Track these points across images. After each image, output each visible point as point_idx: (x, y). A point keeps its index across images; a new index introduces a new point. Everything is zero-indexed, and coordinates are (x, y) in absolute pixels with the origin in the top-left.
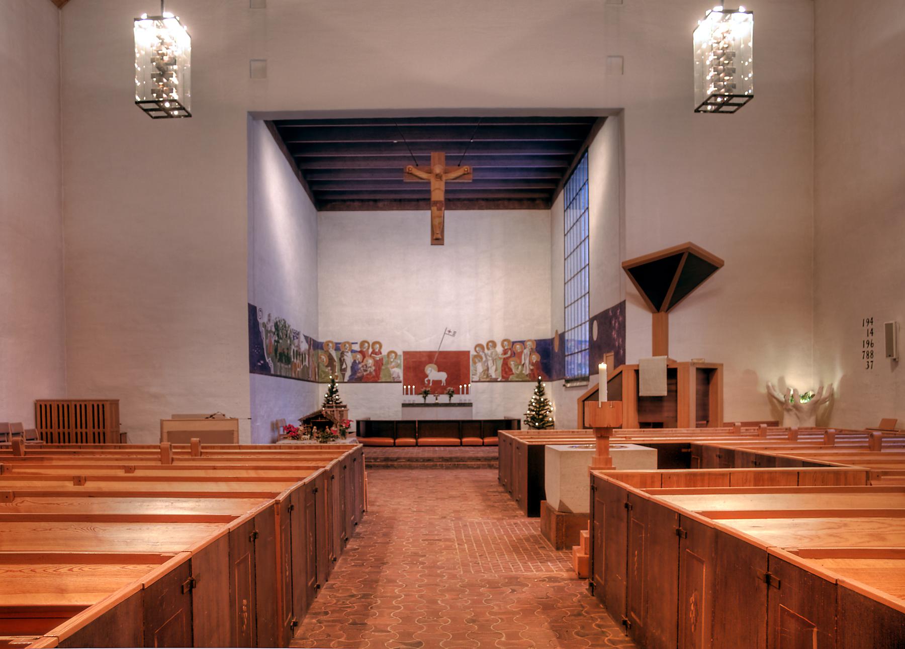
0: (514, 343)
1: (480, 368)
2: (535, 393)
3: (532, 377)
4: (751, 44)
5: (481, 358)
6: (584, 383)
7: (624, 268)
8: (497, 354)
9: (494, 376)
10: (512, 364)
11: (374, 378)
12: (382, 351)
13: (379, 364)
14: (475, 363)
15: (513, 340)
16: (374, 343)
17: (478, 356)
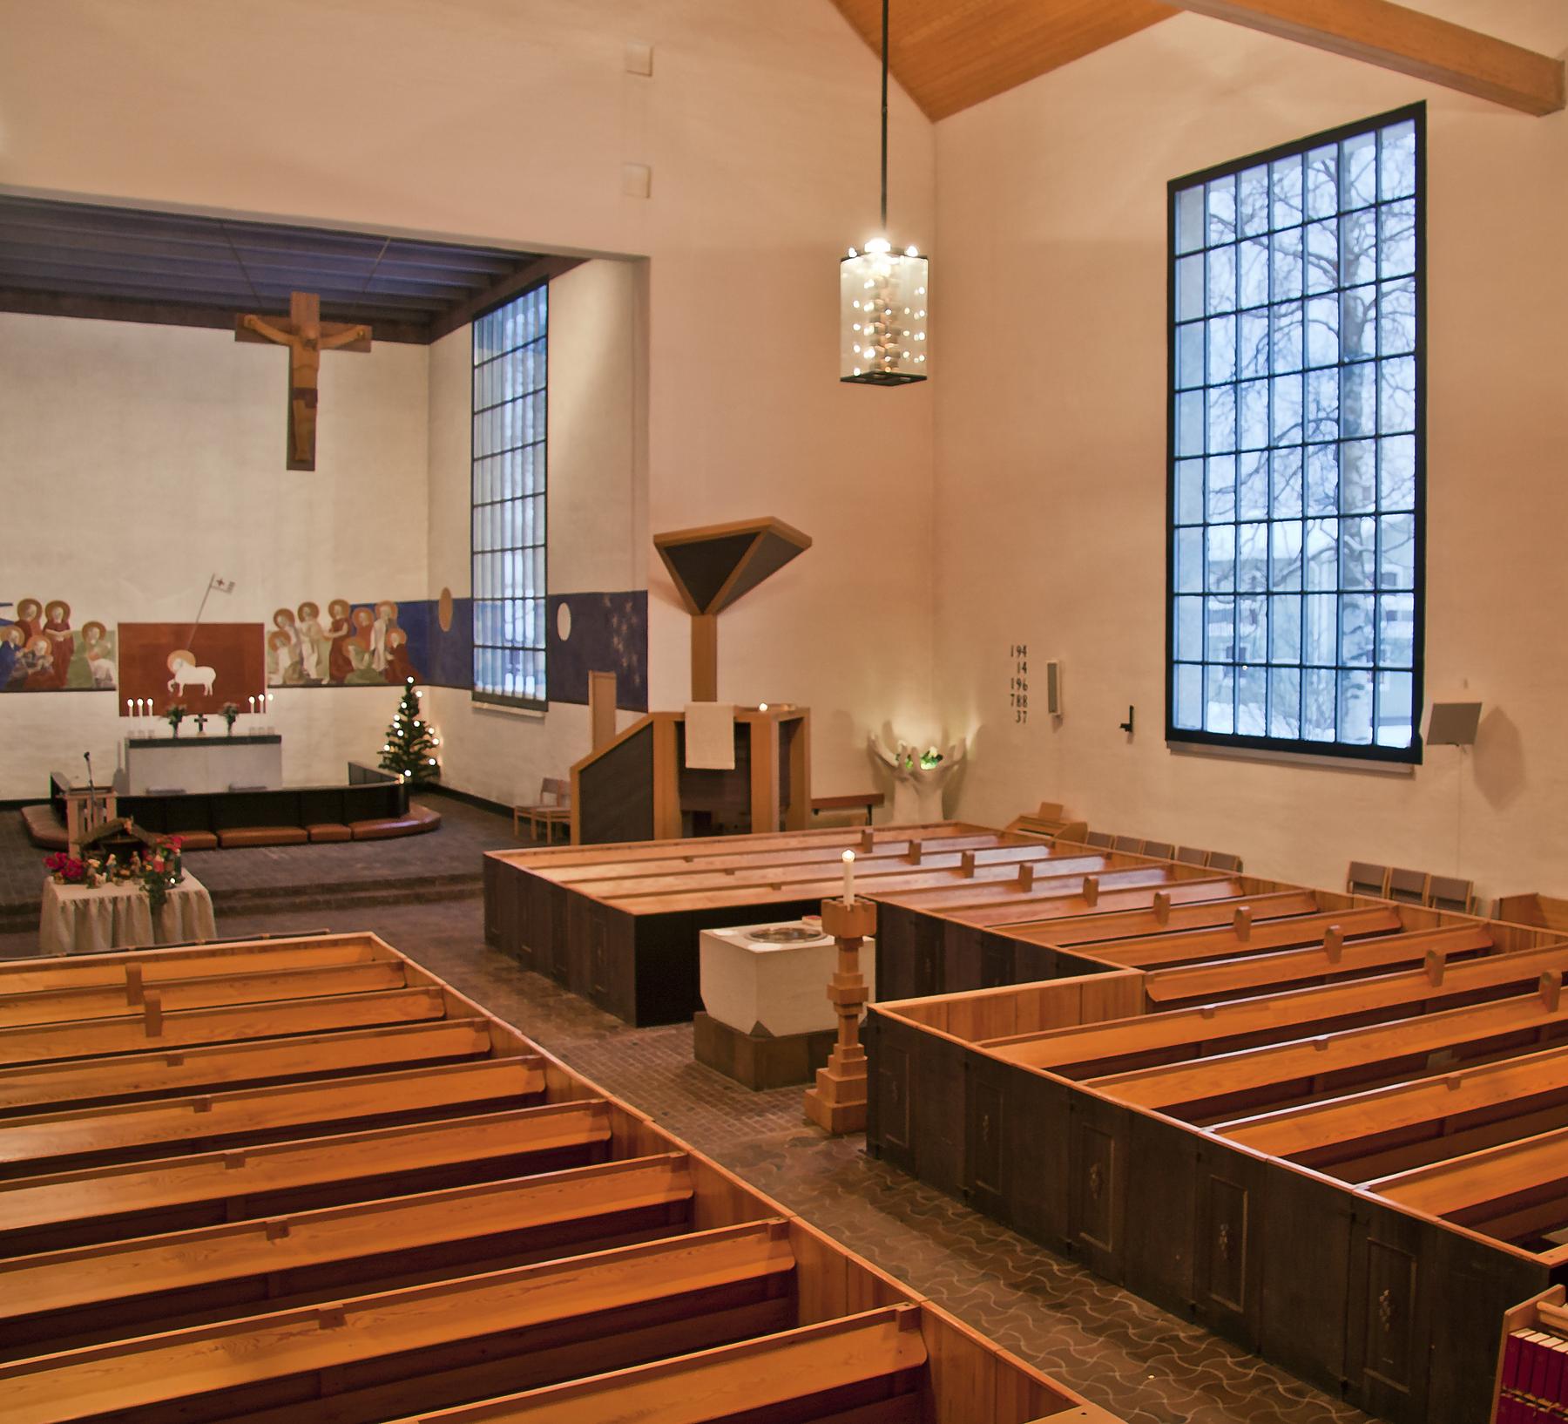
0: (354, 607)
1: (285, 658)
2: (401, 711)
3: (391, 677)
4: (922, 291)
5: (288, 638)
6: (538, 714)
7: (657, 545)
8: (320, 630)
9: (314, 675)
10: (351, 649)
11: (54, 680)
12: (71, 622)
13: (63, 652)
14: (274, 648)
15: (352, 602)
16: (53, 605)
17: (282, 635)
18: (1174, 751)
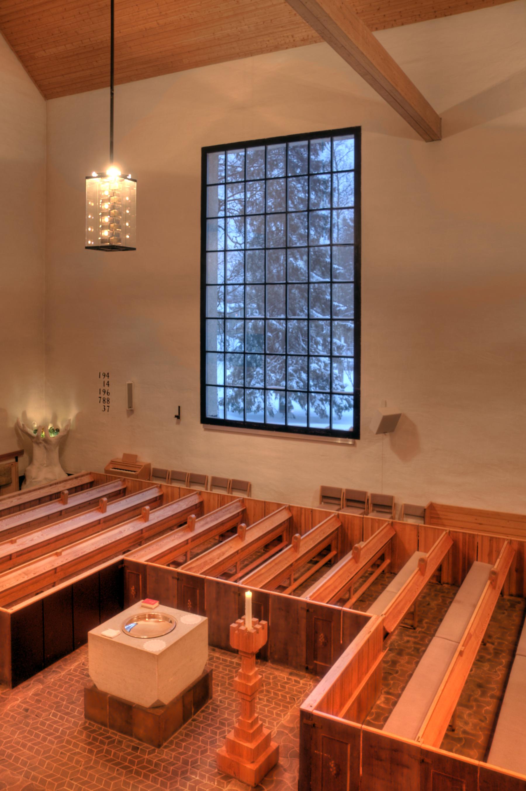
18: (206, 429)
